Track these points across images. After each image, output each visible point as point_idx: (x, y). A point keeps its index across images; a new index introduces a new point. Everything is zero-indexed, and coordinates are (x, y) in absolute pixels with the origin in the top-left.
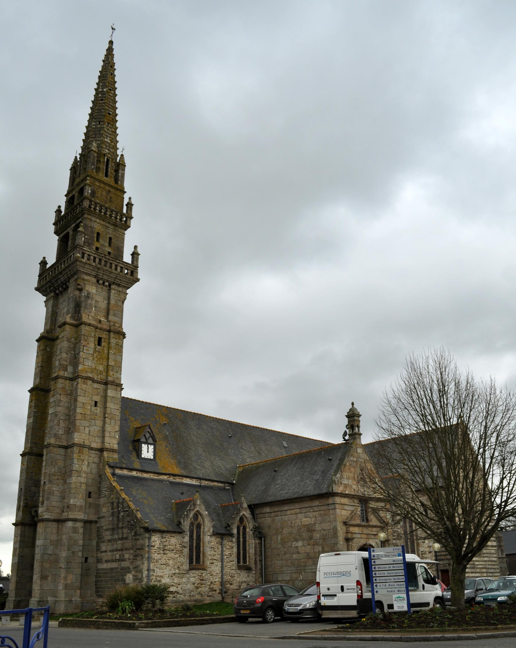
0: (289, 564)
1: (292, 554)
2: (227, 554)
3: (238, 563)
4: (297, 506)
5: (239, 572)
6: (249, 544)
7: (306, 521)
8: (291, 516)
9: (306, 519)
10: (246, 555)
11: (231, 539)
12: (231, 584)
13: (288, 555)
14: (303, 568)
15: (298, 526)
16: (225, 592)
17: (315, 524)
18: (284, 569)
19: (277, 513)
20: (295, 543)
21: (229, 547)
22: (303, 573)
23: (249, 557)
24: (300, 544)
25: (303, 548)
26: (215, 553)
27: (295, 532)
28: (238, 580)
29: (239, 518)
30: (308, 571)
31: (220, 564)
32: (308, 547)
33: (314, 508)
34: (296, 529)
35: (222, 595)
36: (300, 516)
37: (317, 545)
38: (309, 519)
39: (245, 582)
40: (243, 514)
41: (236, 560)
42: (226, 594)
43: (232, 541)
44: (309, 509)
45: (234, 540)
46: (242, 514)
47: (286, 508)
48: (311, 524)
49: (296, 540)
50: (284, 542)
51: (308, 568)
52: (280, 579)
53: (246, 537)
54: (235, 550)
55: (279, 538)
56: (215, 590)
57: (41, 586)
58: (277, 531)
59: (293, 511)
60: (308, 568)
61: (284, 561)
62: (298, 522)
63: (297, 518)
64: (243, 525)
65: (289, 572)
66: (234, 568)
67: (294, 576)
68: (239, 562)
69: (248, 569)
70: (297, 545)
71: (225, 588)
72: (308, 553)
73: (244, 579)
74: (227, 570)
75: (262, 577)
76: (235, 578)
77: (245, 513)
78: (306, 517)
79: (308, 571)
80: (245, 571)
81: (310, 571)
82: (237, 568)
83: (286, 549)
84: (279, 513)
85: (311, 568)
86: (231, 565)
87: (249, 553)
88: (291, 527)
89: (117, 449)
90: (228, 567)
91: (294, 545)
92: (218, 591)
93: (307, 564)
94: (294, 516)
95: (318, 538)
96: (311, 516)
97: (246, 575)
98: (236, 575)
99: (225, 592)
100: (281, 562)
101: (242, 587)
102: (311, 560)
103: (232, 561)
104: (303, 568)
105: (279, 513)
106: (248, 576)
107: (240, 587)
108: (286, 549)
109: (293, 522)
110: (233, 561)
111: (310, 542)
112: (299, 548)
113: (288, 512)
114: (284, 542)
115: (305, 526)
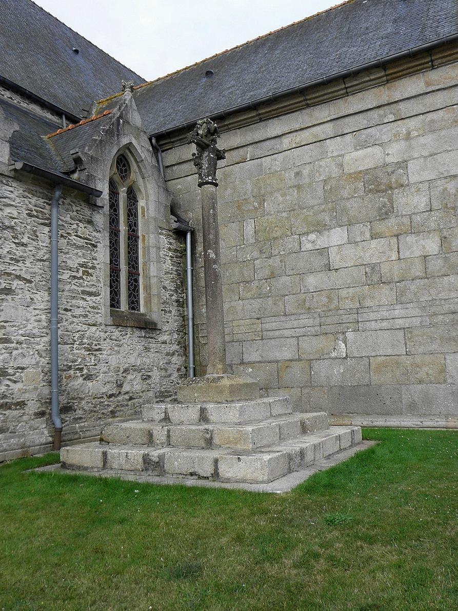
0: (289, 309)
1: (301, 275)
2: (70, 263)
3: (112, 306)
4: (322, 113)
5: (116, 333)
6: (147, 249)
7: (362, 159)
8: (296, 152)
9: (361, 153)
10: (136, 281)
11: (87, 212)
12: (88, 377)
13: (284, 279)
14: (352, 317)
15: (325, 182)
16: (66, 409)
17: (403, 164)
18: (267, 326)
19: (241, 151)
20: (312, 237)
21: (81, 242)
22: (350, 335)
23: (148, 288)
24: (337, 236)
25: (350, 251)
26: (19, 252)
27: (313, 202)
28: (114, 361)
29: (115, 151)
30: (373, 325)
31: (42, 298)
32: (374, 243)
33: (402, 106)
34: (320, 193)
35: (50, 422)
36: (333, 146)
37: (418, 233)
38: (377, 150)
39: (135, 369)
40: (129, 146)
41: (105, 292)
42: (69, 417)
43: (90, 222)
44: (375, 114)
45: (101, 219)
46: (125, 141)
47: (275, 127)
48: (386, 165)
49: (321, 228)
50: (266, 241)
51: (372, 316)
52: (253, 356)
53: (136, 224)
54: (103, 255)
55: (249, 228)
56: (22, 404)
57: (335, 386)
58: (239, 207)
59: (306, 133)
60: (372, 316)
61: (270, 301)
62: (328, 168)
63: (324, 154)
64: (128, 182)
65: (287, 333)
66: (100, 320)
67: (310, 346)
68: (114, 302)
69: (148, 327)
70: (322, 242)
71: (60, 392)
72: (374, 267)
73: (132, 360)
74: (72, 324)
75: (186, 354)
76: (103, 356)
77: (134, 142)
78: (363, 145)
79: (373, 325)
80: (137, 333)
81: (385, 324)
82: (110, 322)
83: (275, 262)
84: (249, 152)
85: (385, 314)
86: (90, 307)
87: (148, 278)
88: (299, 187)
89: (53, 439)
90: (78, 312)
91: (309, 246)
92: (33, 407)
93: (368, 303)
94: (308, 153)
95: (422, 206)
96: (385, 138)
97: (140, 347)
98: (105, 345)
99: (66, 409)
100: (256, 304)
101: (126, 387)
102: (385, 290)
103: (90, 294)
104: (352, 317)
105: (250, 149)
106: (147, 349)
107: (120, 386)
108: (275, 262)
109: (306, 172)
110: (96, 294)
111: (380, 227)
112: (333, 252)
113: (286, 142)
114: (266, 241)
115: (356, 176)
